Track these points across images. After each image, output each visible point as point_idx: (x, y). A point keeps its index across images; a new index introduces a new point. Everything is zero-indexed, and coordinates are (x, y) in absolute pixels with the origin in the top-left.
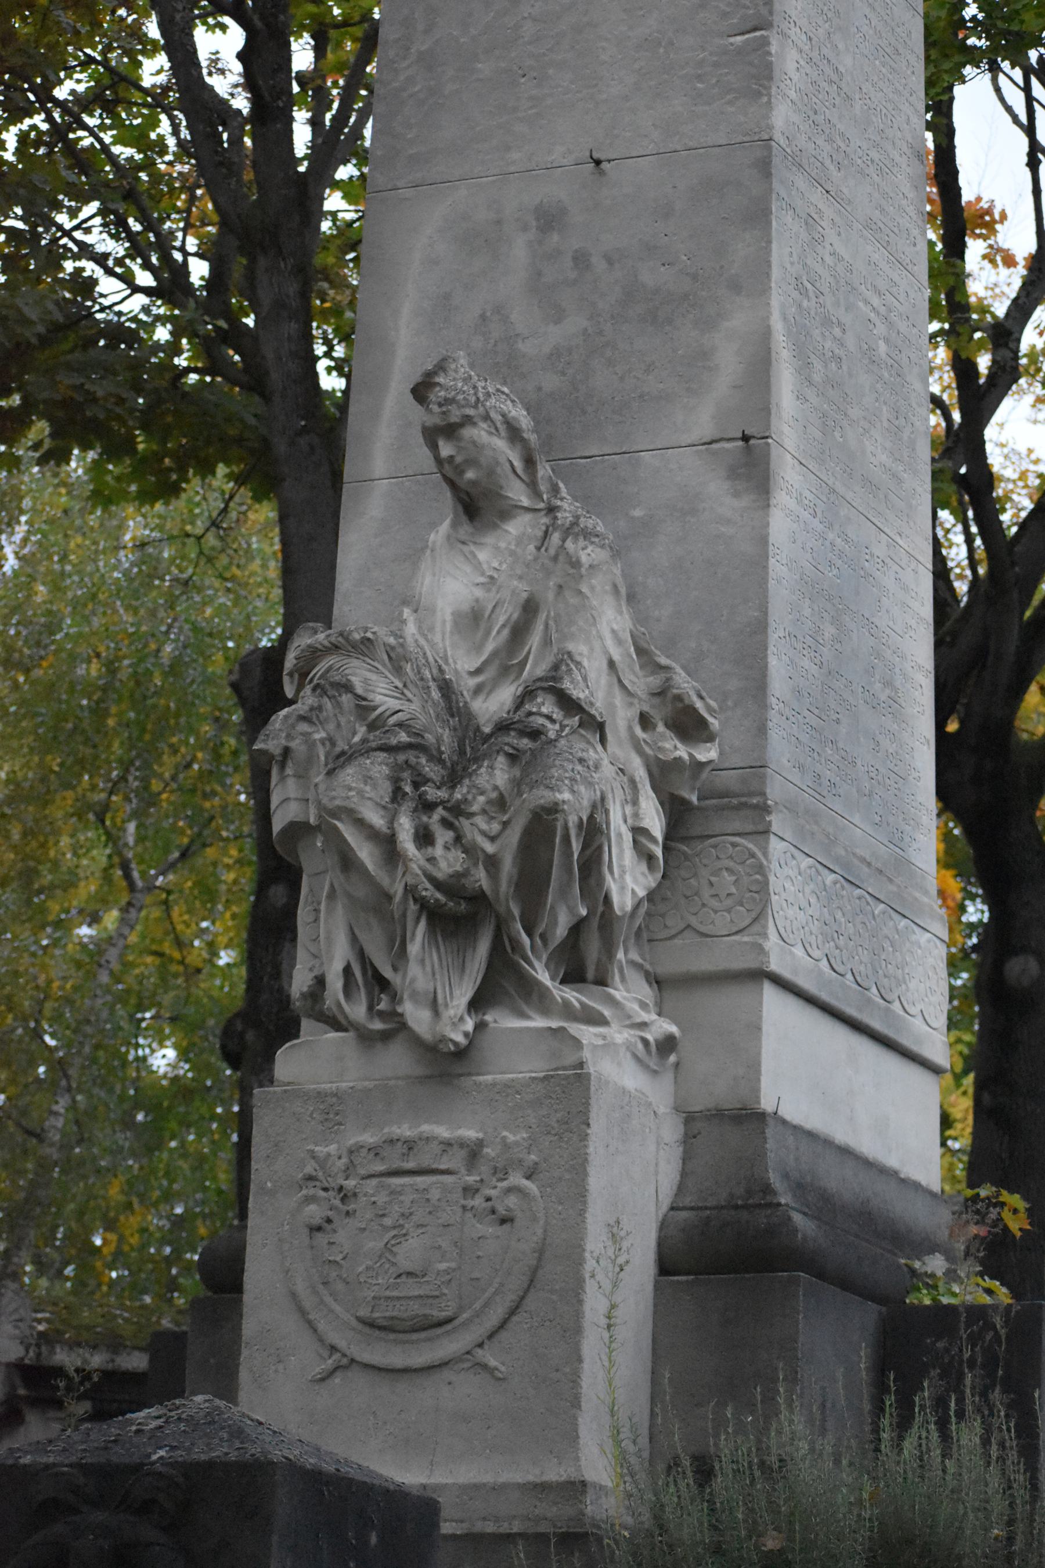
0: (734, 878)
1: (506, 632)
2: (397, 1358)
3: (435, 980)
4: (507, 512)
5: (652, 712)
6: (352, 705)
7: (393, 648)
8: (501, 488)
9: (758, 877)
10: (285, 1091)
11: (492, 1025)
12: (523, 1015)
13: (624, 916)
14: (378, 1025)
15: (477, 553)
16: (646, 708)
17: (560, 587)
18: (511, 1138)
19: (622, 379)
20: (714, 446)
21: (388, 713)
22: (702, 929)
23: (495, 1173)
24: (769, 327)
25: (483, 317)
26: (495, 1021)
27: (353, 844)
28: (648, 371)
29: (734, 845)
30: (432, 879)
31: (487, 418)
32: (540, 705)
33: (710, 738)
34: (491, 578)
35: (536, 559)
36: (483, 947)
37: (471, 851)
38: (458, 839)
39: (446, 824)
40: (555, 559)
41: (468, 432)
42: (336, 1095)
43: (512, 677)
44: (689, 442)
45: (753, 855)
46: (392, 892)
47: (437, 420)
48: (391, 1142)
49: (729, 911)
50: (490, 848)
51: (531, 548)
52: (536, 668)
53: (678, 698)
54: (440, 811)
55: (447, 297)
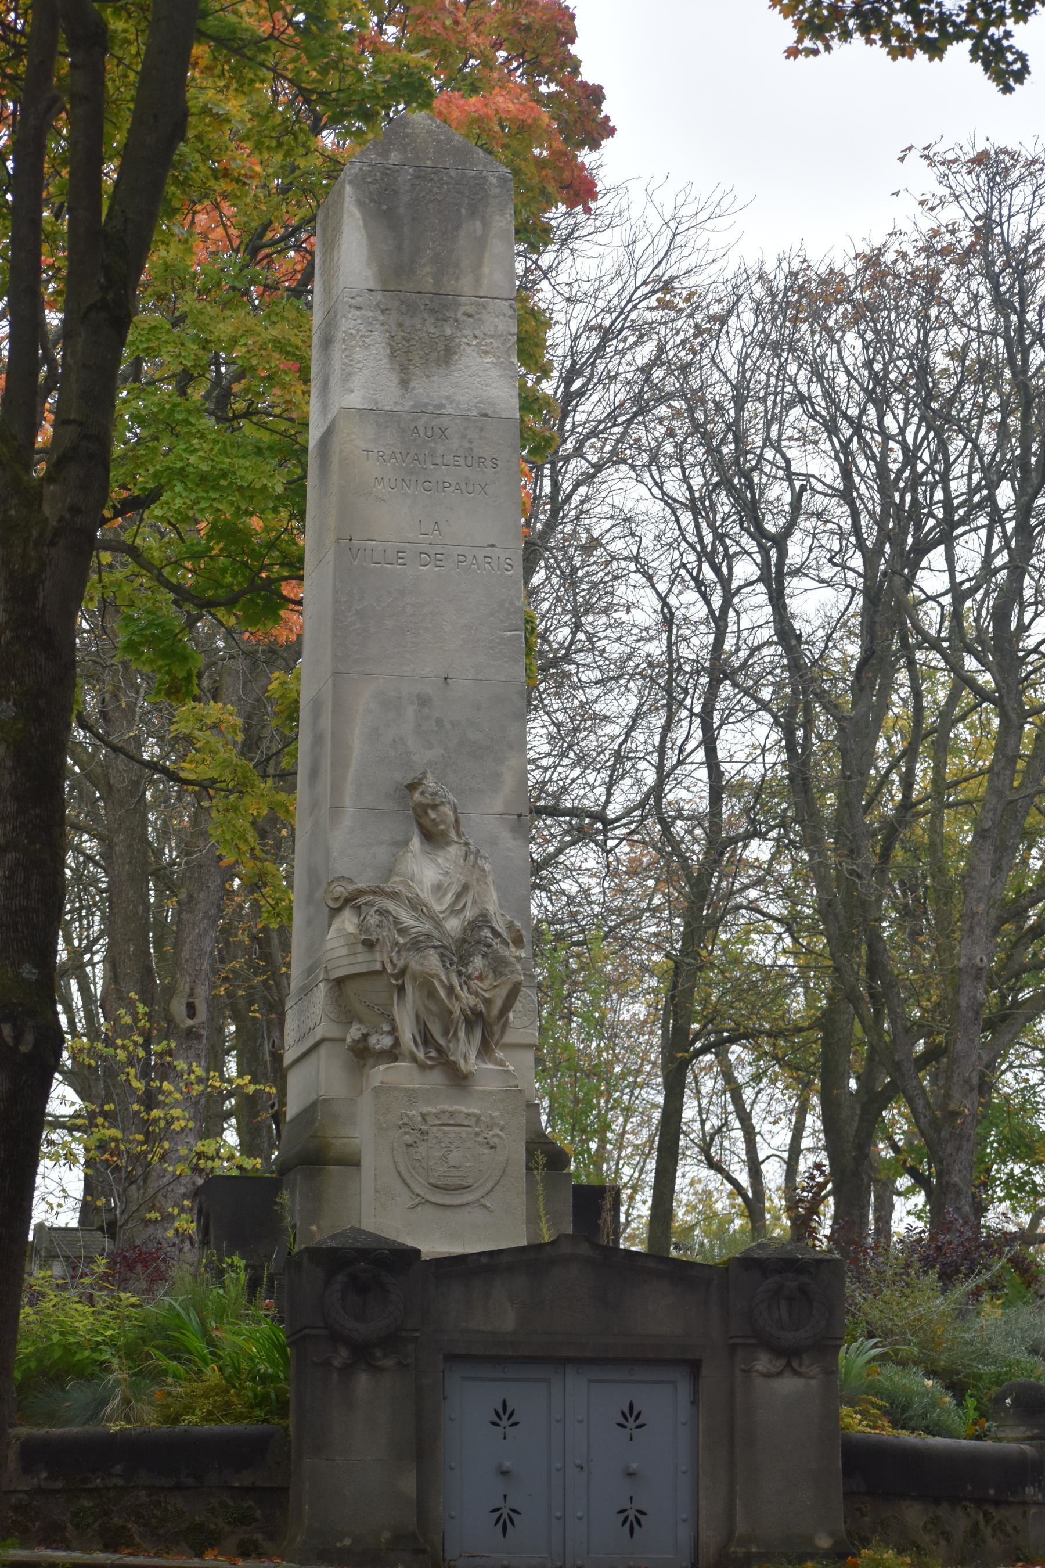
2: (447, 1200)
4: (448, 843)
14: (430, 1063)
48: (444, 1112)
50: (487, 995)
52: (469, 914)
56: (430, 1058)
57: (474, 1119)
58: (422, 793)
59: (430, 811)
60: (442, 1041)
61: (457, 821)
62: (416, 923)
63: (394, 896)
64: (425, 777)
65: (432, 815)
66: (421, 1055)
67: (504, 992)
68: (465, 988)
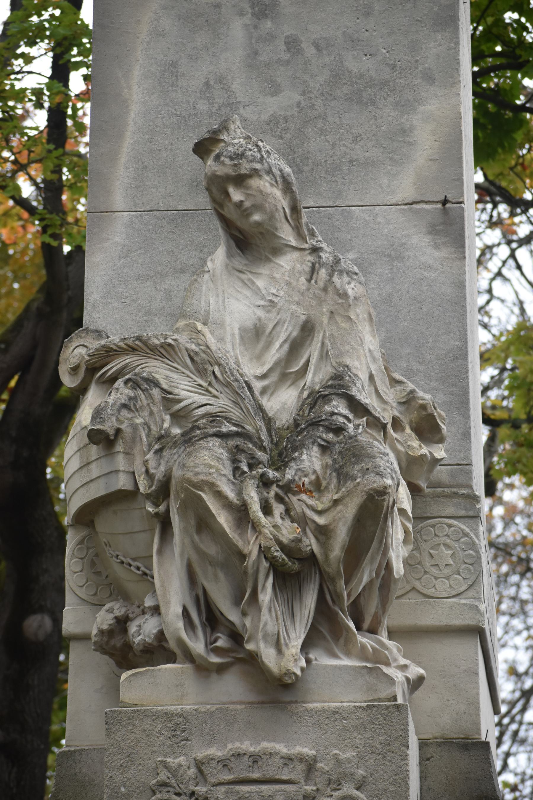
0: (450, 552)
1: (286, 347)
3: (278, 624)
4: (278, 250)
5: (402, 417)
6: (159, 397)
7: (197, 354)
8: (276, 229)
9: (471, 552)
10: (135, 711)
11: (314, 662)
12: (335, 656)
13: (400, 578)
14: (215, 659)
15: (255, 280)
16: (396, 413)
17: (332, 312)
18: (343, 756)
19: (333, 146)
20: (415, 206)
21: (194, 406)
22: (425, 591)
23: (329, 784)
24: (460, 113)
25: (207, 84)
26: (316, 659)
27: (214, 511)
28: (356, 140)
29: (450, 526)
30: (279, 543)
31: (270, 172)
32: (336, 407)
33: (441, 440)
34: (271, 301)
35: (308, 289)
36: (310, 600)
37: (302, 521)
38: (287, 511)
39: (279, 499)
40: (325, 289)
41: (255, 183)
42: (181, 716)
43: (289, 383)
44: (394, 201)
45: (466, 535)
46: (246, 551)
47: (229, 171)
48: (239, 755)
49: (448, 578)
50: (321, 521)
51: (303, 280)
52: (315, 378)
53: (423, 407)
54: (274, 489)
55: (174, 65)
56: (217, 651)
57: (301, 767)
58: (217, 158)
59: (231, 190)
60: (233, 615)
61: (295, 209)
62: (203, 399)
63: (166, 351)
64: (224, 127)
65: (236, 195)
66: (198, 646)
67: (349, 512)
68: (278, 509)
